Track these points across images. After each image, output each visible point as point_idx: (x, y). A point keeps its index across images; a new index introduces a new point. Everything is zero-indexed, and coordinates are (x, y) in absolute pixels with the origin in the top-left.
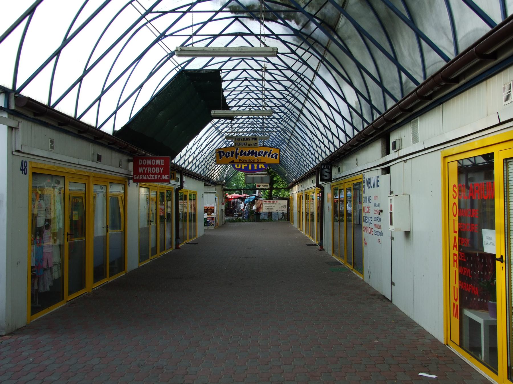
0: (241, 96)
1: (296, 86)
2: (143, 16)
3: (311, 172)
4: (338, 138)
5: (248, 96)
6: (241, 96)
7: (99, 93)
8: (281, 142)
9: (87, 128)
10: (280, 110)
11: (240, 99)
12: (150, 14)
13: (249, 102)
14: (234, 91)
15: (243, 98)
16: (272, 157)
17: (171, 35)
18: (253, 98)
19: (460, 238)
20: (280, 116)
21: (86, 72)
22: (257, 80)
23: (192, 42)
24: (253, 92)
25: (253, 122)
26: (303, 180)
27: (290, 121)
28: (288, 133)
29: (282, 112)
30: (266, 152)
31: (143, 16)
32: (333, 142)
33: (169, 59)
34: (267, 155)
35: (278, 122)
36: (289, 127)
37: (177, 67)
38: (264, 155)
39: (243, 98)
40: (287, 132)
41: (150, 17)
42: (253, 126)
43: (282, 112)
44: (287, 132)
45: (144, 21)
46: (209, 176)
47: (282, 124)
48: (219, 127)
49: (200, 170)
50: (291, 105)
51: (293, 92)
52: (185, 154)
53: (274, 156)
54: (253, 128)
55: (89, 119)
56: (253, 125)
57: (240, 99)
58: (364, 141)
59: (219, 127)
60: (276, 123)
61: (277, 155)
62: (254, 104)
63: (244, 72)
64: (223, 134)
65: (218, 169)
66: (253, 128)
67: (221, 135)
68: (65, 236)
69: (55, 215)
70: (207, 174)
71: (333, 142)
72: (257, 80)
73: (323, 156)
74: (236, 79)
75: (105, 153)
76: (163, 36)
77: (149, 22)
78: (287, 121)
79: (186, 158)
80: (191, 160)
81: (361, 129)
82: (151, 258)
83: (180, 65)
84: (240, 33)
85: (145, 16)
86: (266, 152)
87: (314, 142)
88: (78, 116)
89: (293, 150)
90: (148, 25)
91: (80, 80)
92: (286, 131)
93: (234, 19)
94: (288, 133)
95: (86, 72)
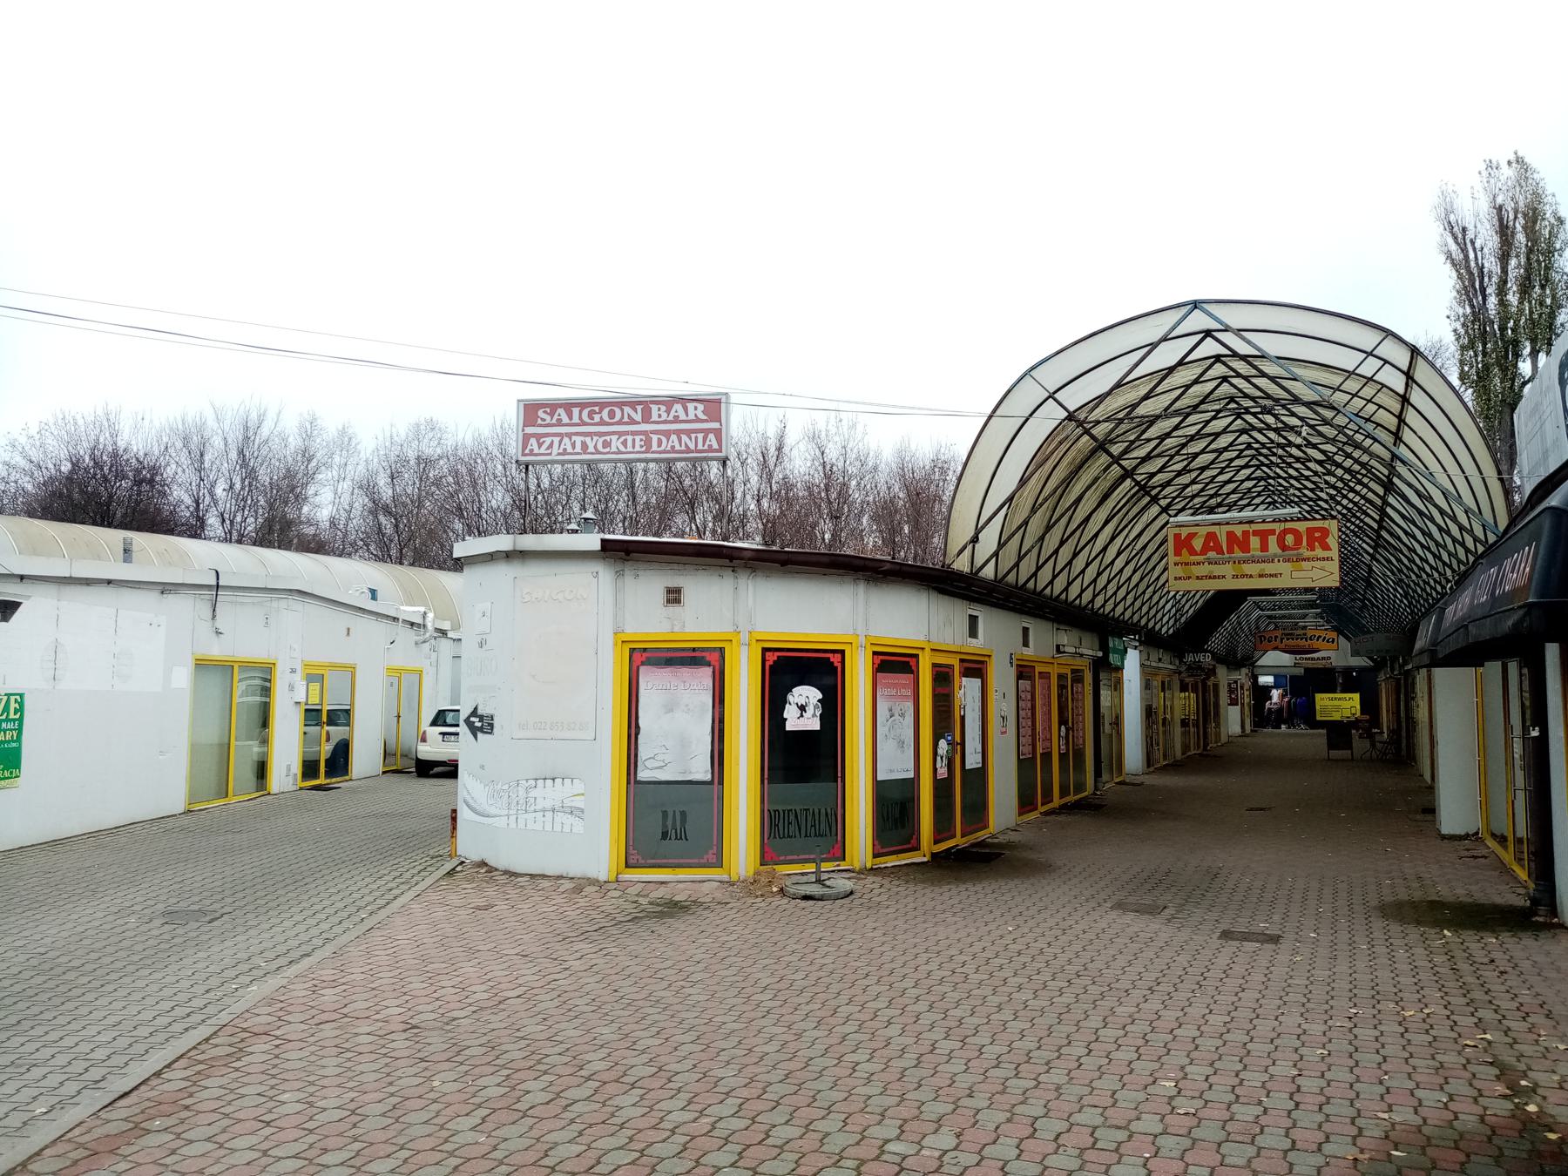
8: (1360, 508)
9: (959, 576)
13: (1244, 438)
14: (1224, 468)
15: (1224, 431)
16: (1328, 641)
18: (1239, 375)
19: (940, 690)
25: (1237, 403)
28: (1372, 485)
30: (1320, 637)
34: (1321, 640)
36: (1373, 463)
40: (1371, 479)
44: (1371, 479)
46: (1157, 627)
49: (1130, 610)
52: (1105, 587)
54: (1259, 479)
55: (962, 565)
62: (1258, 442)
65: (1151, 589)
66: (1242, 432)
68: (1426, 719)
70: (1152, 622)
74: (1217, 435)
75: (985, 615)
79: (1135, 609)
80: (1063, 558)
86: (1320, 637)
89: (1392, 541)
92: (1364, 476)
94: (1372, 485)
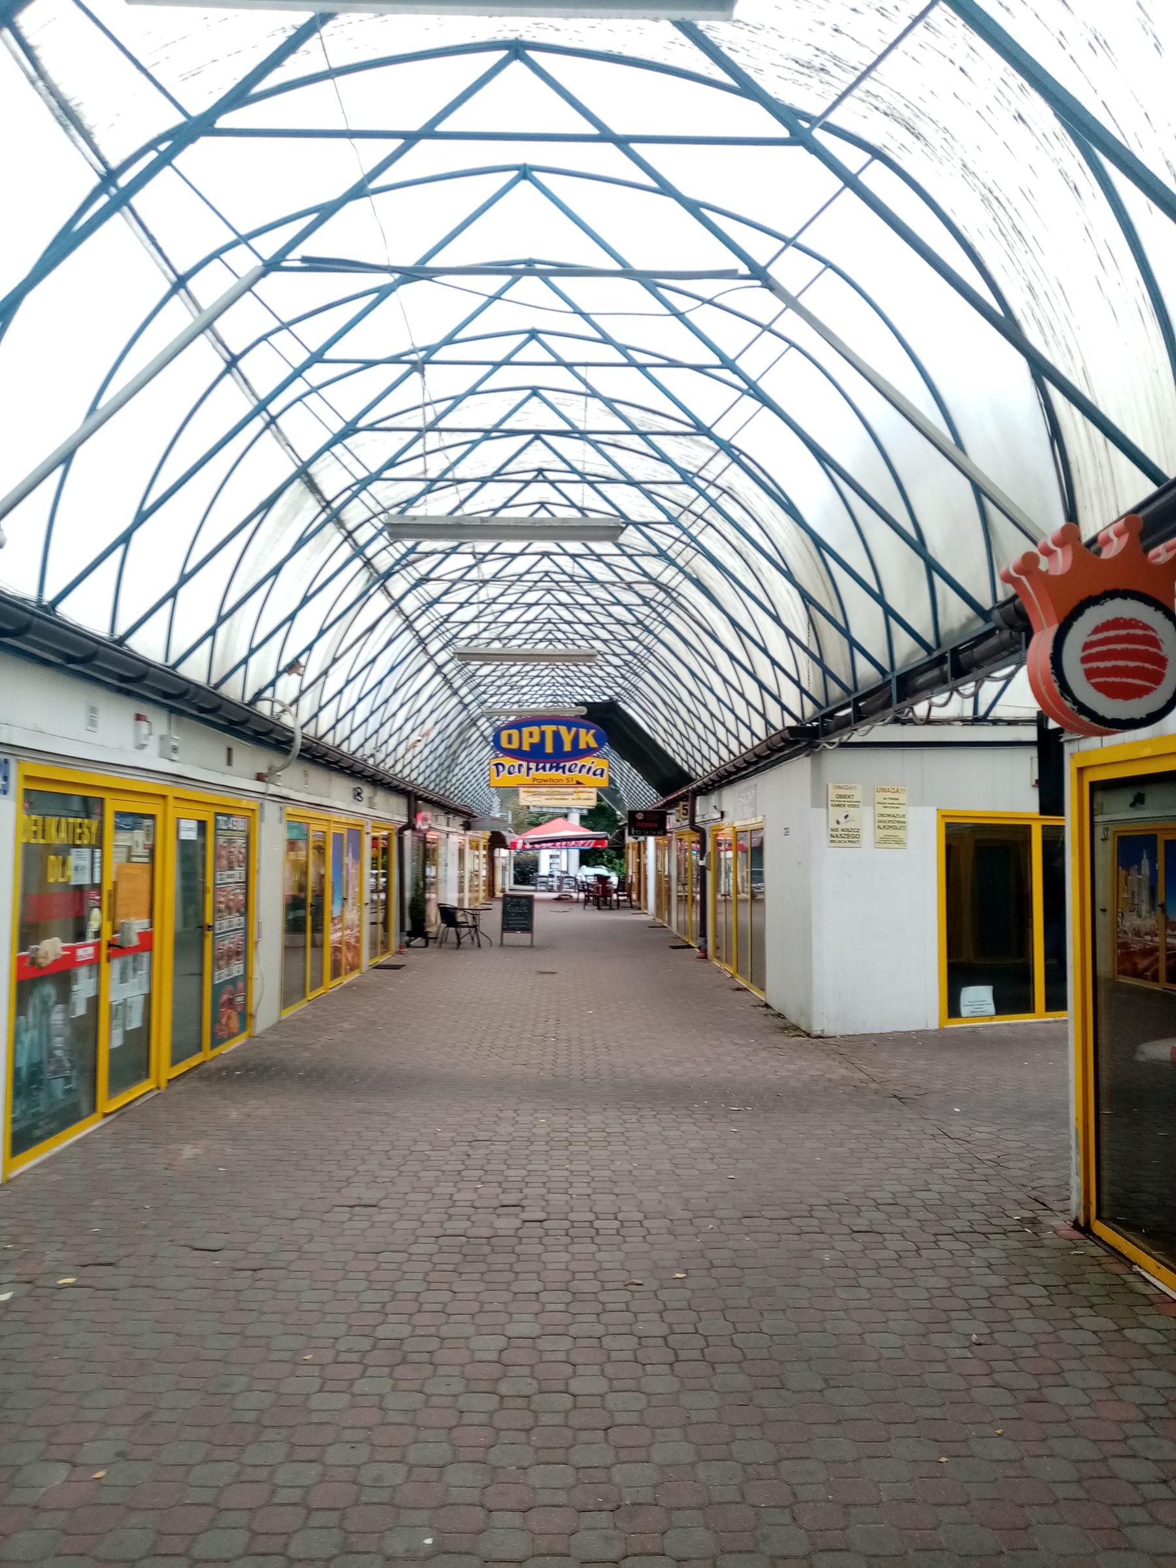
0: (531, 598)
1: (639, 660)
2: (298, 373)
3: (711, 780)
4: (737, 738)
5: (548, 599)
6: (531, 598)
7: (174, 581)
10: (616, 683)
11: (530, 606)
12: (317, 366)
17: (371, 428)
20: (624, 661)
21: (142, 517)
22: (569, 623)
23: (421, 451)
24: (559, 640)
26: (710, 790)
27: (662, 626)
29: (620, 686)
30: (583, 766)
31: (298, 373)
32: (818, 656)
33: (355, 495)
34: (585, 770)
35: (618, 674)
37: (375, 516)
38: (580, 771)
39: (536, 604)
41: (318, 373)
42: (553, 674)
43: (620, 686)
45: (298, 387)
47: (626, 679)
48: (486, 701)
50: (672, 571)
51: (635, 668)
53: (599, 772)
56: (553, 670)
57: (530, 606)
58: (767, 757)
59: (486, 701)
60: (623, 624)
61: (603, 770)
63: (546, 560)
64: (478, 681)
67: (473, 685)
69: (575, 895)
71: (818, 656)
72: (569, 623)
73: (742, 739)
76: (350, 429)
77: (314, 390)
78: (645, 651)
81: (750, 746)
82: (108, 1104)
83: (385, 511)
84: (530, 262)
85: (303, 370)
87: (694, 730)
88: (49, 596)
90: (312, 399)
91: (125, 539)
93: (503, 53)
95: (142, 517)
